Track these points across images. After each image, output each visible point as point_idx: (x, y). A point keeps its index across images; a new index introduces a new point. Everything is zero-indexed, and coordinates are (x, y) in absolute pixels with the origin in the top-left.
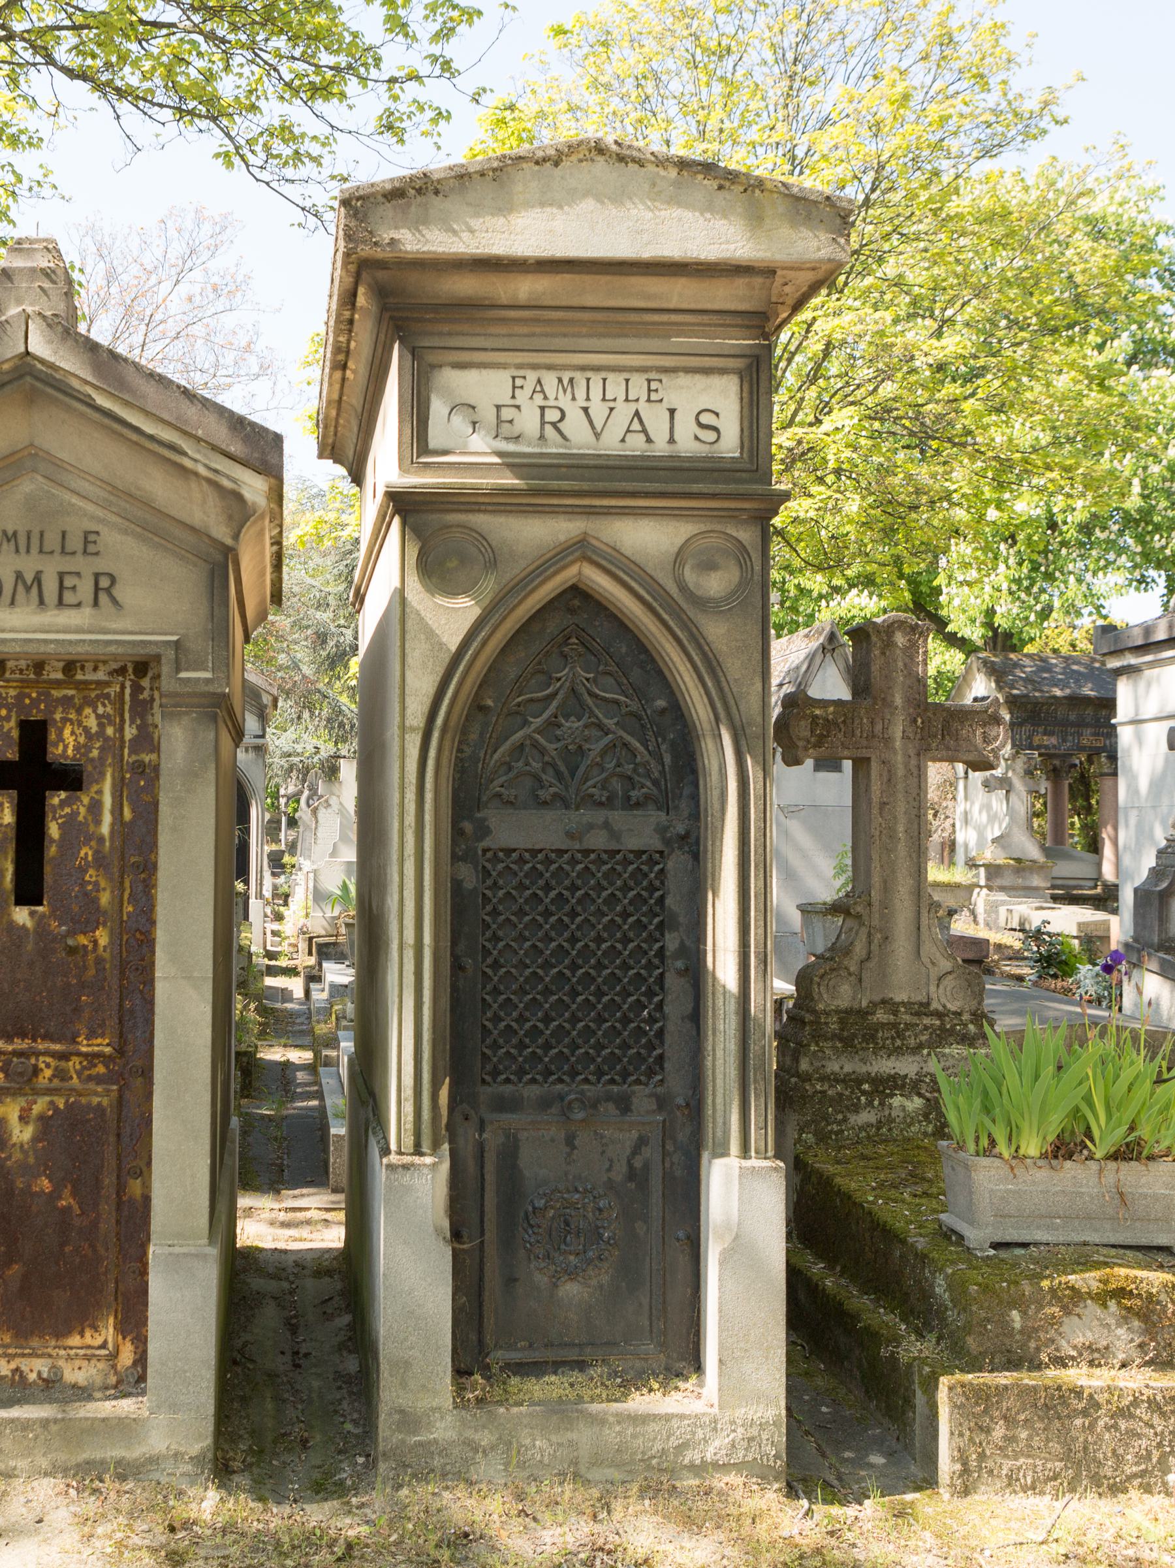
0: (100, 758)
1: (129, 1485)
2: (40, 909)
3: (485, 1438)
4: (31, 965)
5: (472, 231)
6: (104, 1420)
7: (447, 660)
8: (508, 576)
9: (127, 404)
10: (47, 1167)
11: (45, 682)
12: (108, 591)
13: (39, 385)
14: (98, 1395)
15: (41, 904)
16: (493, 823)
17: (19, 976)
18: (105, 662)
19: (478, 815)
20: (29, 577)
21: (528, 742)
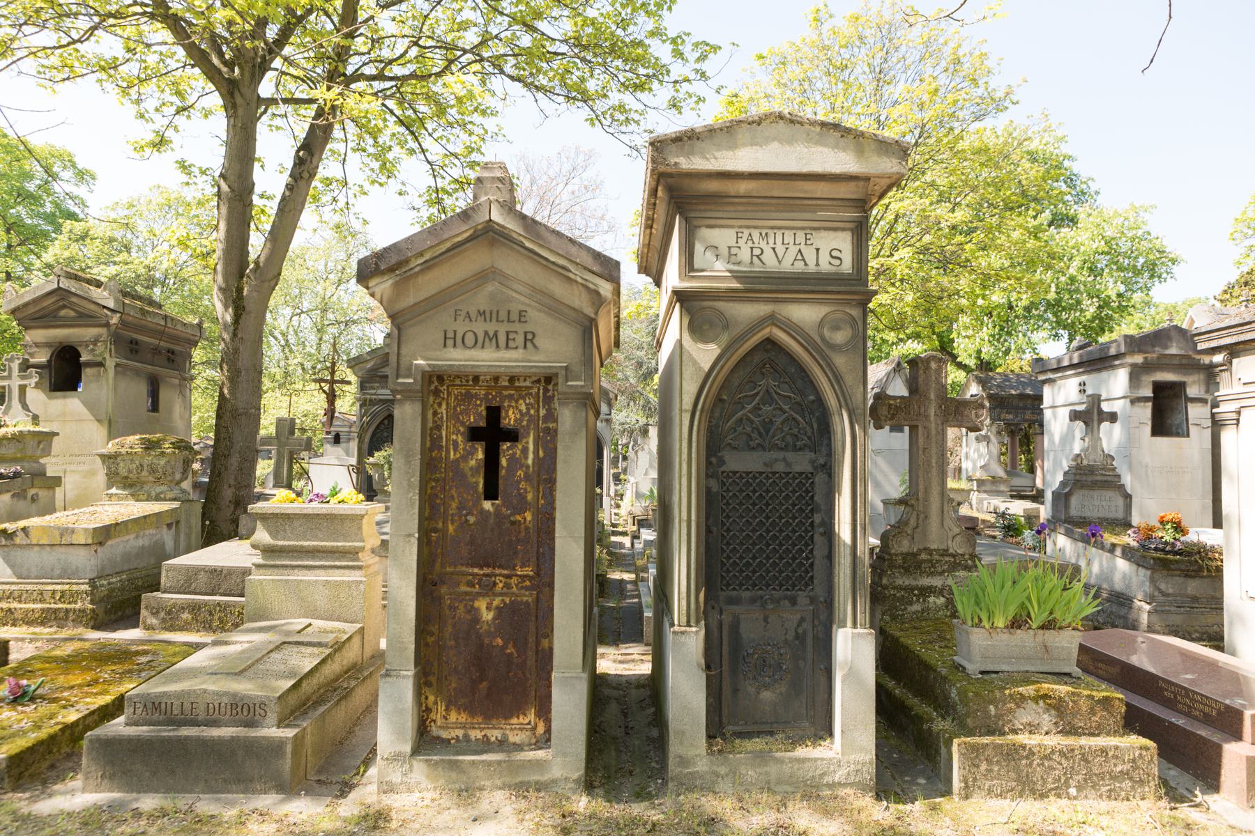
1: (542, 794)
3: (723, 770)
4: (492, 530)
9: (541, 246)
12: (531, 341)
16: (727, 458)
20: (491, 334)
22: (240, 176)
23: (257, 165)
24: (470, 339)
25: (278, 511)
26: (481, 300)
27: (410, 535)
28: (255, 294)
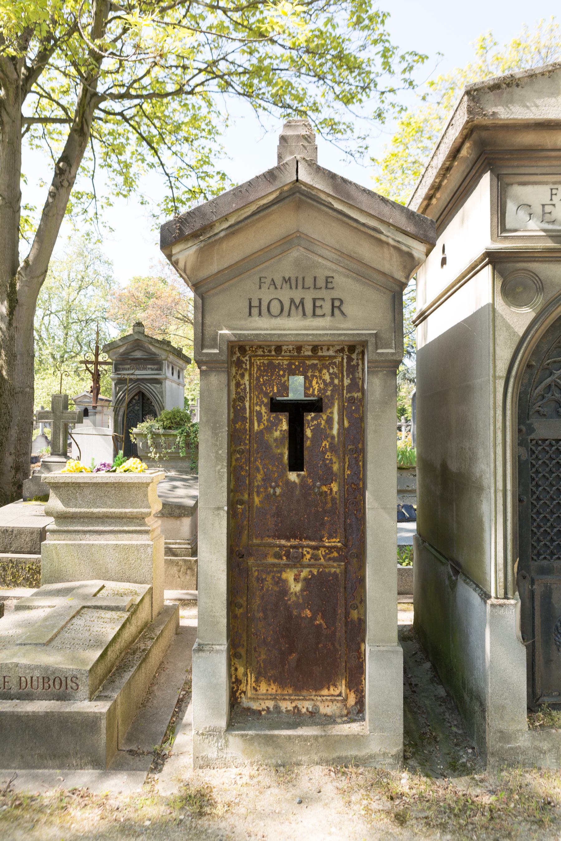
0: (331, 395)
1: (361, 770)
2: (302, 473)
3: (545, 746)
4: (298, 501)
5: (537, 106)
6: (346, 736)
7: (518, 341)
8: (550, 296)
9: (351, 206)
10: (308, 604)
11: (303, 356)
12: (339, 308)
13: (303, 198)
14: (339, 720)
15: (303, 470)
16: (536, 425)
17: (292, 507)
18: (333, 346)
19: (528, 422)
20: (297, 301)
21: (553, 384)
22: (9, 186)
23: (22, 180)
24: (275, 307)
25: (69, 480)
26: (286, 266)
27: (219, 508)
28: (26, 289)
